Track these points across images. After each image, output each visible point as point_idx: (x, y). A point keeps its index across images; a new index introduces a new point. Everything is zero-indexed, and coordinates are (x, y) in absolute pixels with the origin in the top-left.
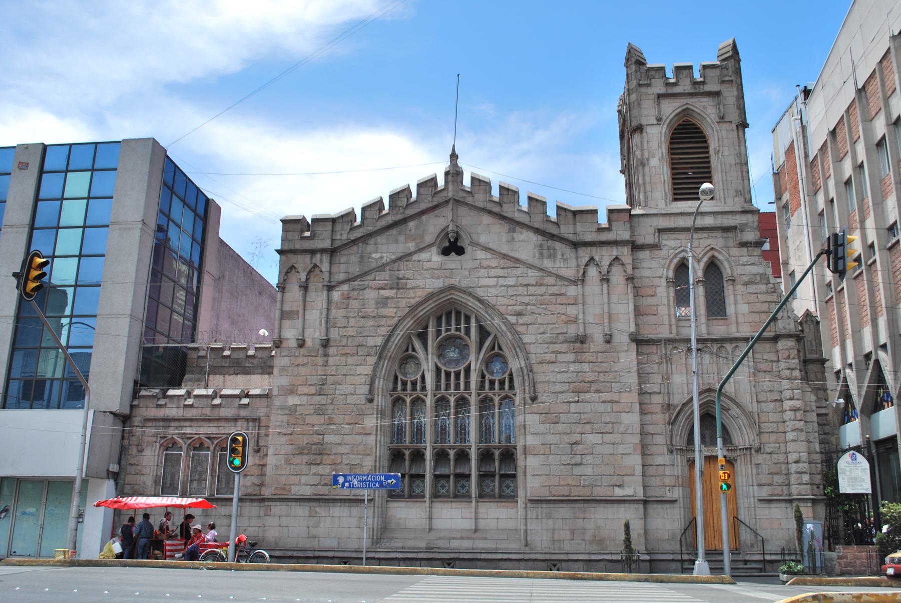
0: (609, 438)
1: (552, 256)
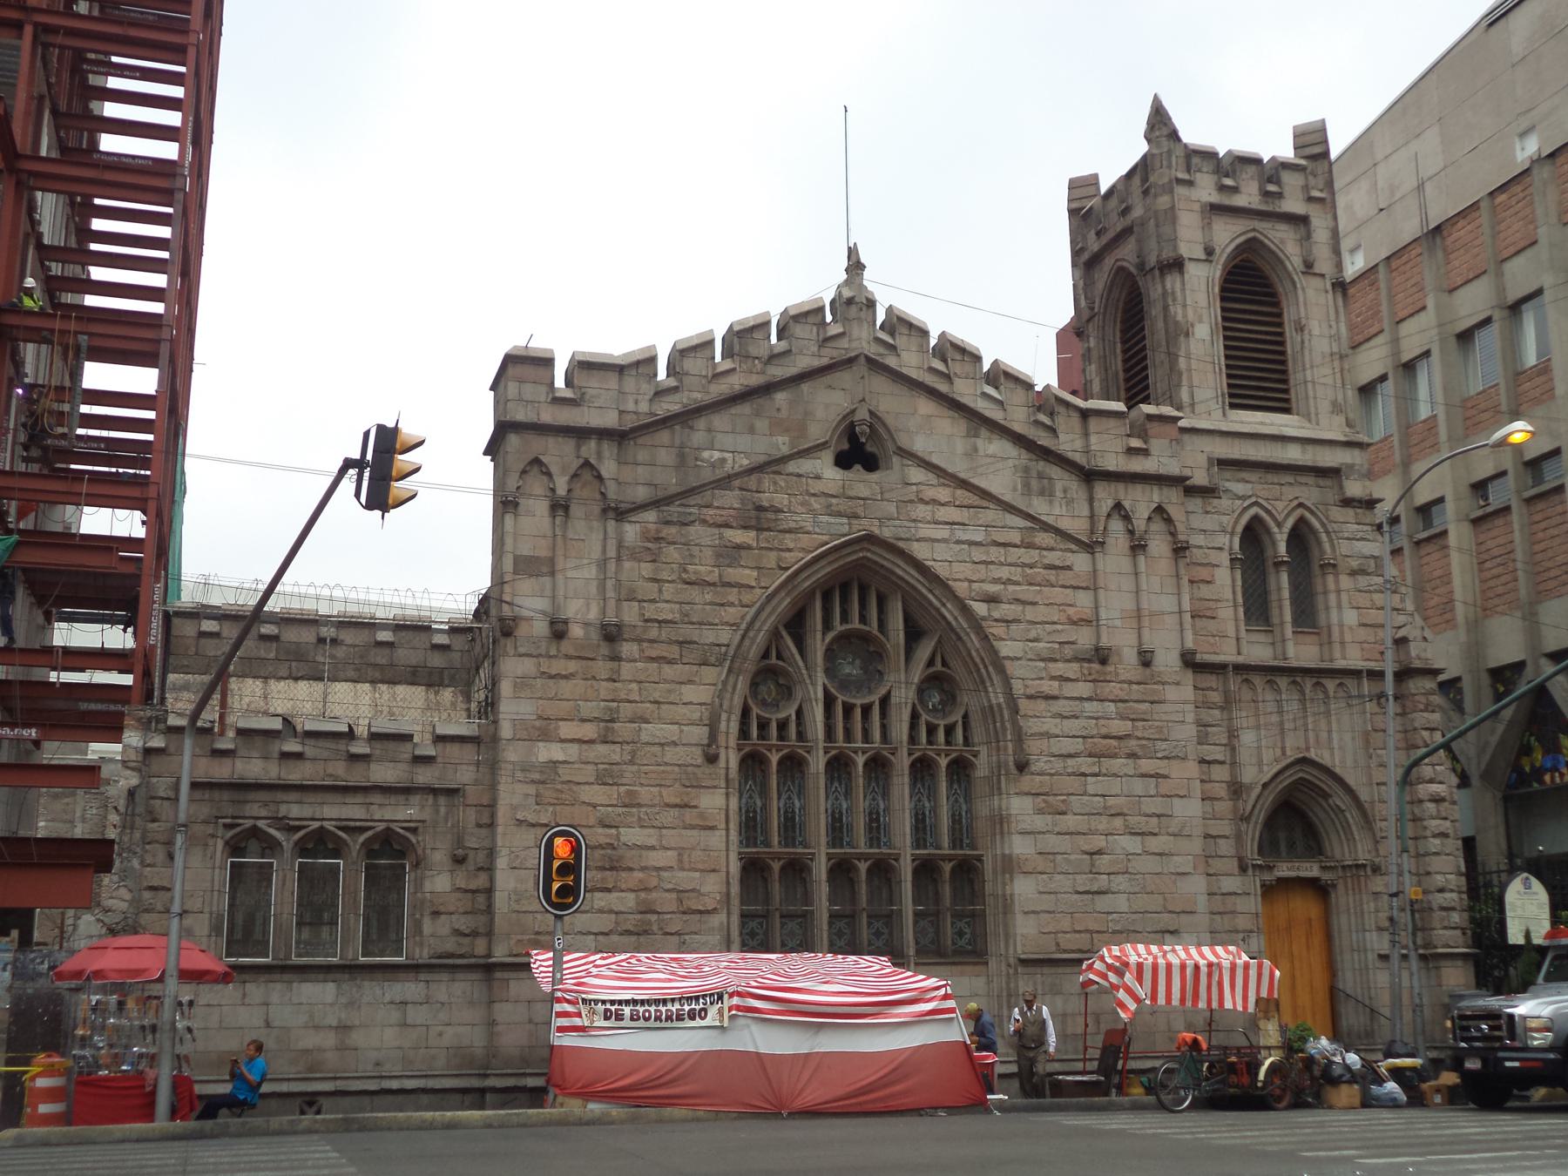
0: (1154, 844)
1: (1047, 493)
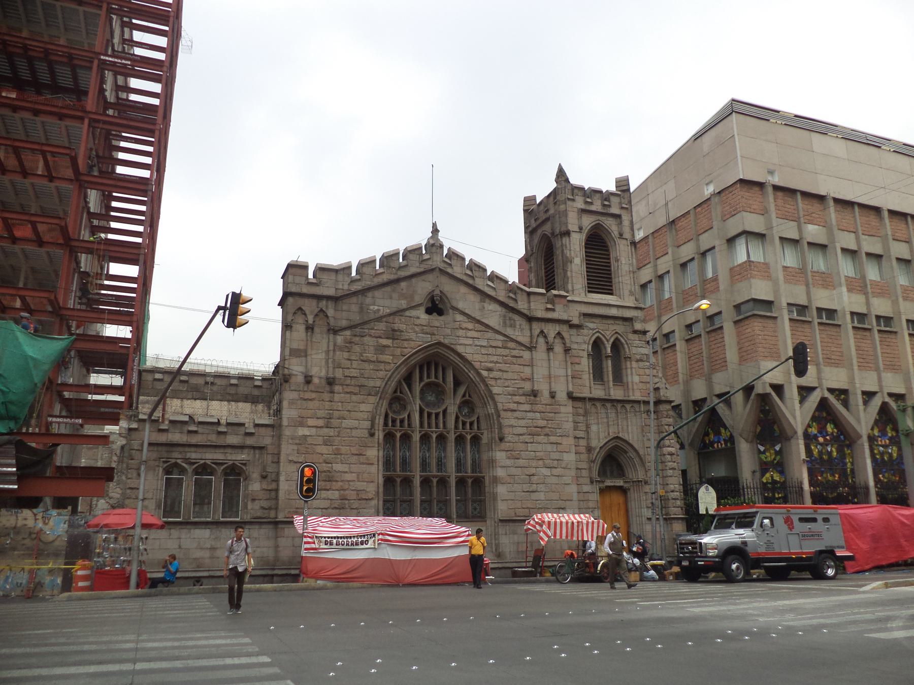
0: (555, 472)
1: (513, 326)
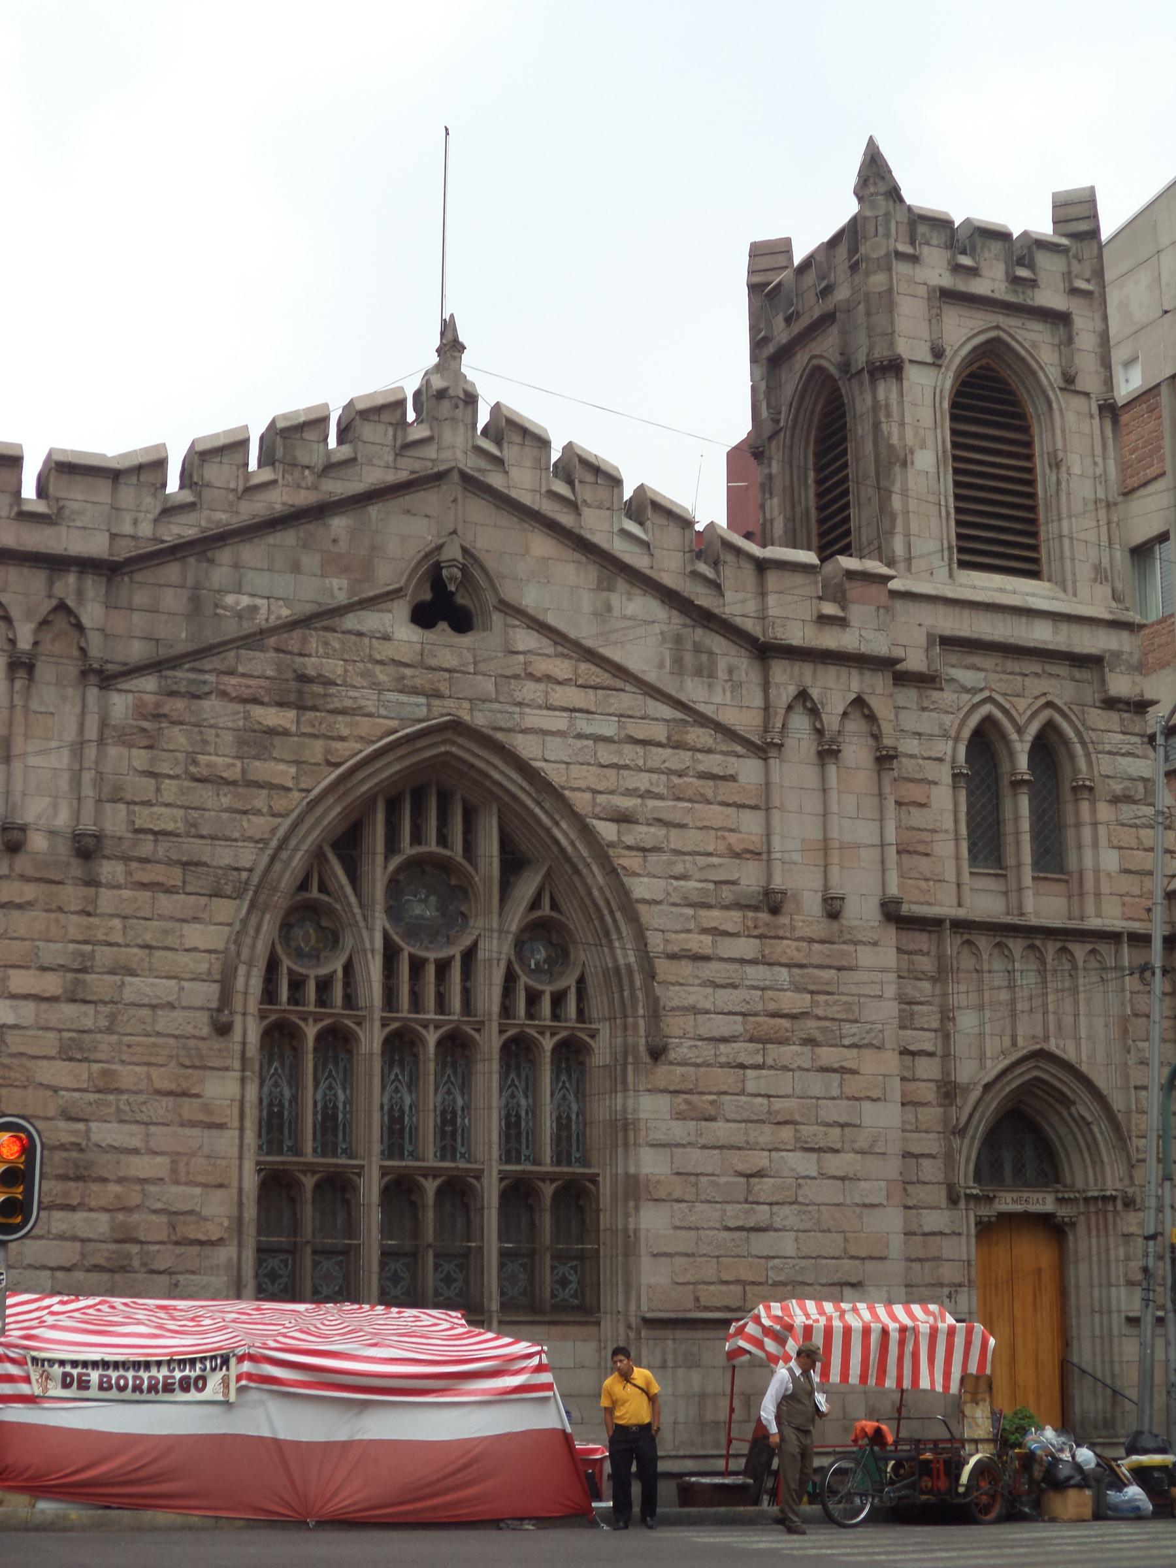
0: (836, 1164)
1: (705, 672)
